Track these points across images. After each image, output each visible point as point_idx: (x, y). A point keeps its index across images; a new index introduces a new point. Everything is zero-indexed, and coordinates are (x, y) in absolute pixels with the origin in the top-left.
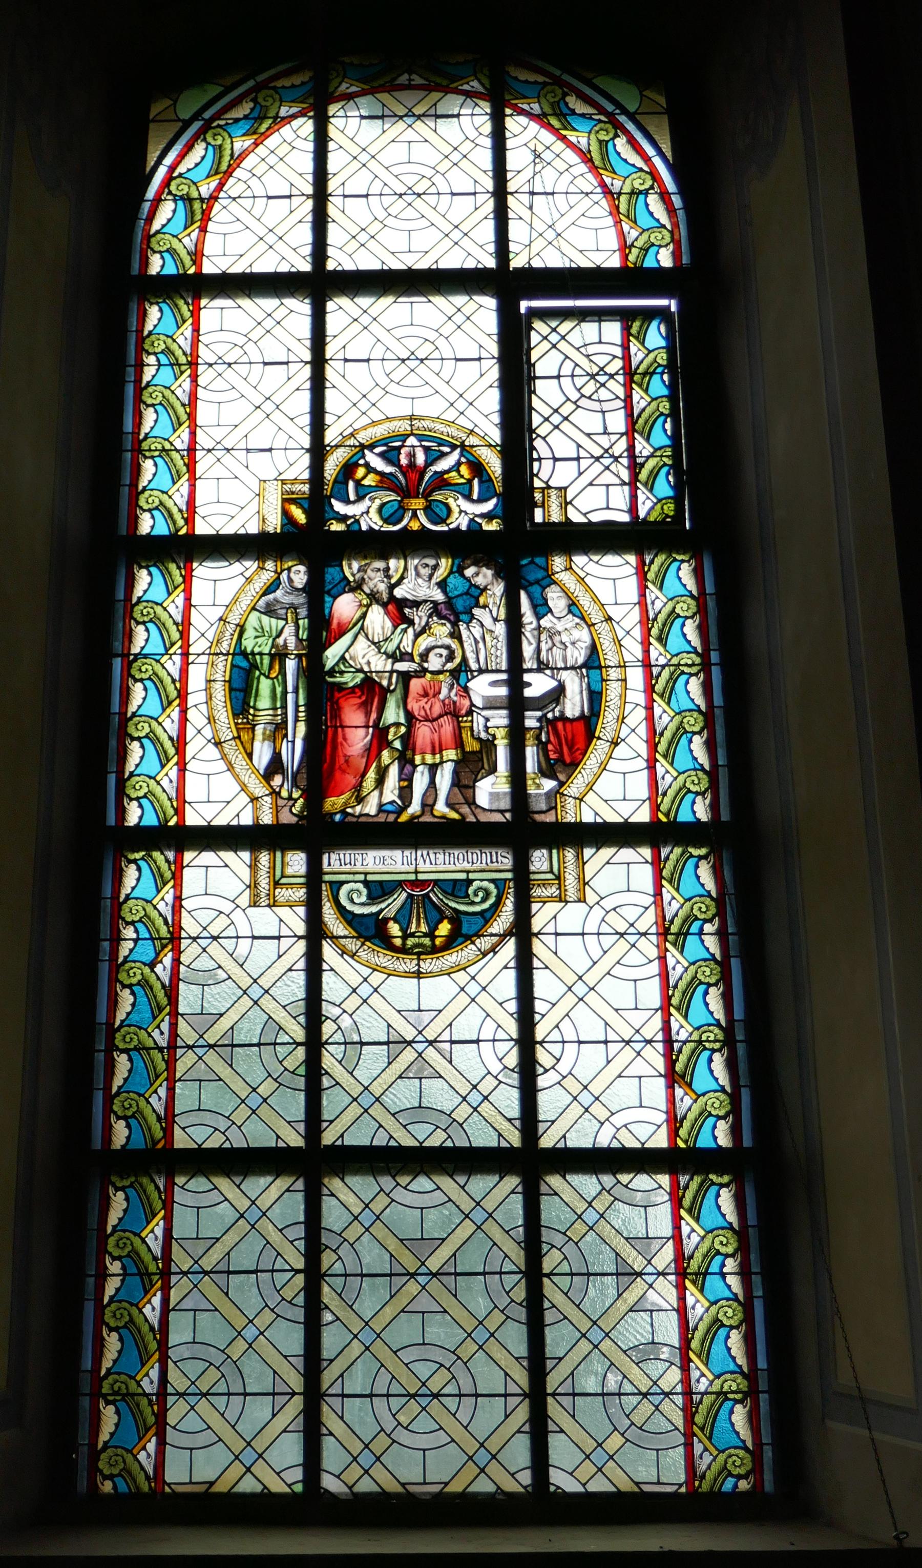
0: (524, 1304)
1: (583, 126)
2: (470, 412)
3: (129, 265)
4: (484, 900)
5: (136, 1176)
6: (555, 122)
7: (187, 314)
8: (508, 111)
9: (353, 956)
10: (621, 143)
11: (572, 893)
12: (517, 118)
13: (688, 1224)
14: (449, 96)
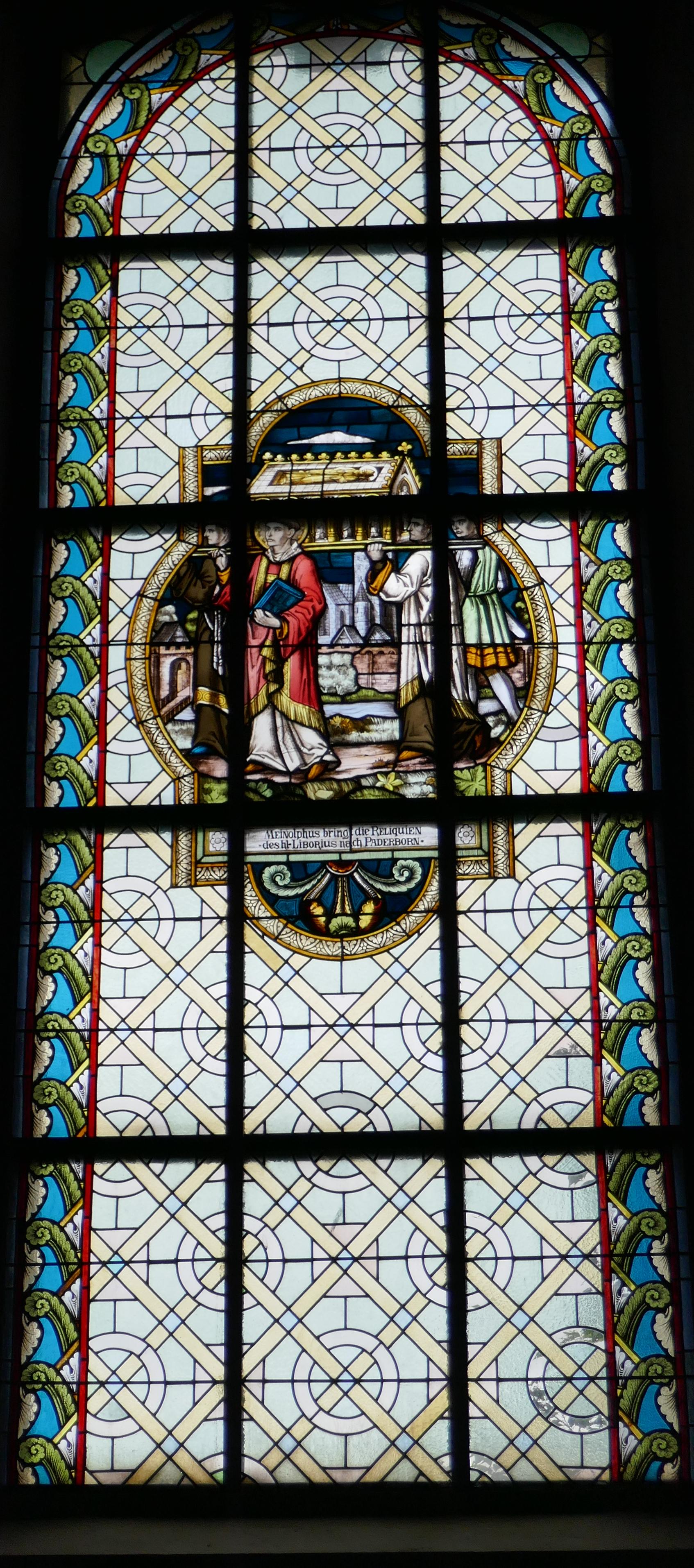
0: (440, 1053)
1: (520, 69)
2: (398, 372)
3: (37, 500)
4: (409, 879)
5: (66, 834)
6: (489, 66)
7: (105, 279)
8: (442, 59)
9: (276, 939)
10: (559, 87)
11: (502, 869)
12: (452, 65)
13: (608, 1063)
14: (380, 42)
